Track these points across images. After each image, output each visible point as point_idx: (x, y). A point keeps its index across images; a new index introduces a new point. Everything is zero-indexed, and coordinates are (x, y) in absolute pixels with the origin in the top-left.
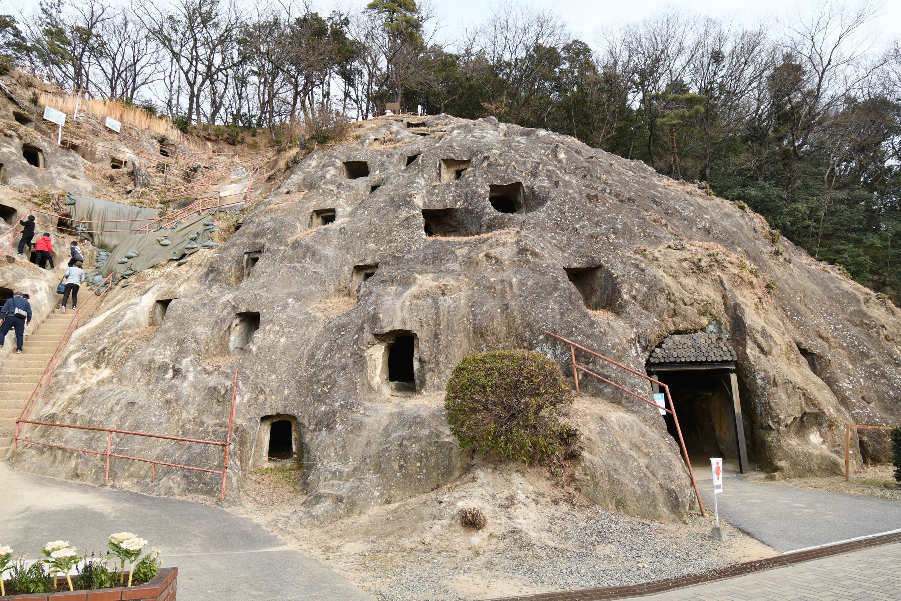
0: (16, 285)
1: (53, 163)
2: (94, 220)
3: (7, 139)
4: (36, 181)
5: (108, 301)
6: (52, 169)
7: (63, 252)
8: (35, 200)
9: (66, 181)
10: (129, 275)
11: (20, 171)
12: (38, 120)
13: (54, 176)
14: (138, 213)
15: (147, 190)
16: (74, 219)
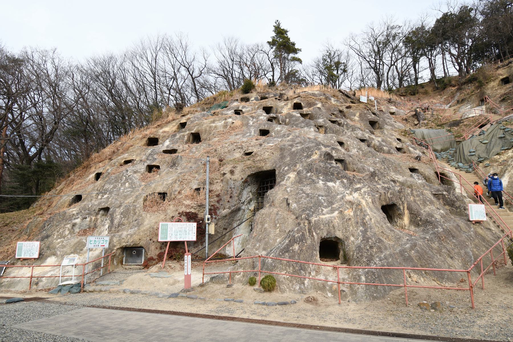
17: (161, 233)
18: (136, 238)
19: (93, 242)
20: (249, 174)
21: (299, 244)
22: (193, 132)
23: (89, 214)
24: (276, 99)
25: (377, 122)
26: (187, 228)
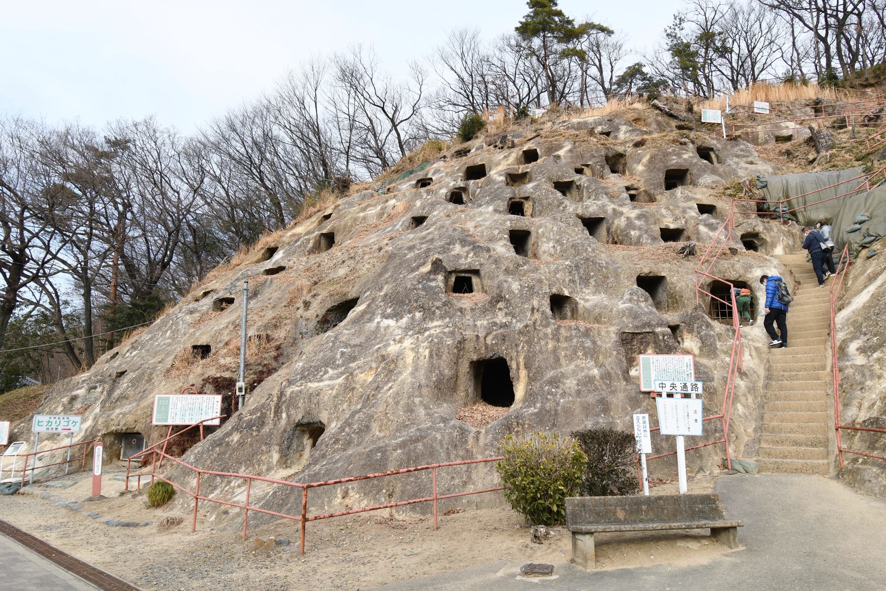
0: (749, 275)
1: (728, 156)
2: (793, 196)
3: (684, 147)
4: (720, 175)
5: (856, 278)
6: (729, 162)
7: (774, 237)
8: (729, 192)
9: (746, 169)
10: (871, 242)
11: (705, 171)
12: (697, 126)
13: (734, 167)
14: (838, 176)
15: (834, 151)
16: (771, 201)
17: (158, 412)
18: (130, 418)
19: (45, 423)
20: (330, 306)
21: (241, 432)
22: (325, 231)
23: (100, 381)
24: (495, 146)
25: (687, 170)
26: (204, 405)
